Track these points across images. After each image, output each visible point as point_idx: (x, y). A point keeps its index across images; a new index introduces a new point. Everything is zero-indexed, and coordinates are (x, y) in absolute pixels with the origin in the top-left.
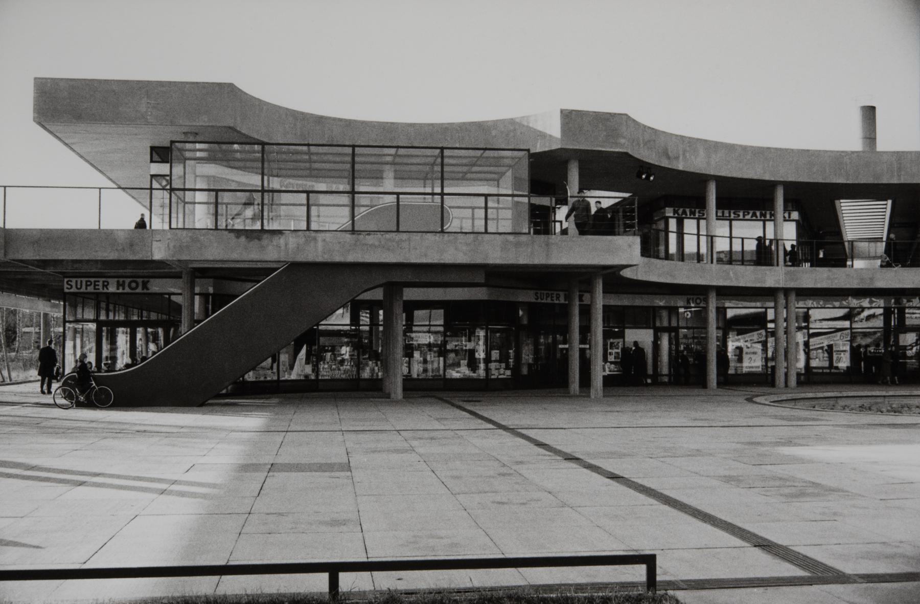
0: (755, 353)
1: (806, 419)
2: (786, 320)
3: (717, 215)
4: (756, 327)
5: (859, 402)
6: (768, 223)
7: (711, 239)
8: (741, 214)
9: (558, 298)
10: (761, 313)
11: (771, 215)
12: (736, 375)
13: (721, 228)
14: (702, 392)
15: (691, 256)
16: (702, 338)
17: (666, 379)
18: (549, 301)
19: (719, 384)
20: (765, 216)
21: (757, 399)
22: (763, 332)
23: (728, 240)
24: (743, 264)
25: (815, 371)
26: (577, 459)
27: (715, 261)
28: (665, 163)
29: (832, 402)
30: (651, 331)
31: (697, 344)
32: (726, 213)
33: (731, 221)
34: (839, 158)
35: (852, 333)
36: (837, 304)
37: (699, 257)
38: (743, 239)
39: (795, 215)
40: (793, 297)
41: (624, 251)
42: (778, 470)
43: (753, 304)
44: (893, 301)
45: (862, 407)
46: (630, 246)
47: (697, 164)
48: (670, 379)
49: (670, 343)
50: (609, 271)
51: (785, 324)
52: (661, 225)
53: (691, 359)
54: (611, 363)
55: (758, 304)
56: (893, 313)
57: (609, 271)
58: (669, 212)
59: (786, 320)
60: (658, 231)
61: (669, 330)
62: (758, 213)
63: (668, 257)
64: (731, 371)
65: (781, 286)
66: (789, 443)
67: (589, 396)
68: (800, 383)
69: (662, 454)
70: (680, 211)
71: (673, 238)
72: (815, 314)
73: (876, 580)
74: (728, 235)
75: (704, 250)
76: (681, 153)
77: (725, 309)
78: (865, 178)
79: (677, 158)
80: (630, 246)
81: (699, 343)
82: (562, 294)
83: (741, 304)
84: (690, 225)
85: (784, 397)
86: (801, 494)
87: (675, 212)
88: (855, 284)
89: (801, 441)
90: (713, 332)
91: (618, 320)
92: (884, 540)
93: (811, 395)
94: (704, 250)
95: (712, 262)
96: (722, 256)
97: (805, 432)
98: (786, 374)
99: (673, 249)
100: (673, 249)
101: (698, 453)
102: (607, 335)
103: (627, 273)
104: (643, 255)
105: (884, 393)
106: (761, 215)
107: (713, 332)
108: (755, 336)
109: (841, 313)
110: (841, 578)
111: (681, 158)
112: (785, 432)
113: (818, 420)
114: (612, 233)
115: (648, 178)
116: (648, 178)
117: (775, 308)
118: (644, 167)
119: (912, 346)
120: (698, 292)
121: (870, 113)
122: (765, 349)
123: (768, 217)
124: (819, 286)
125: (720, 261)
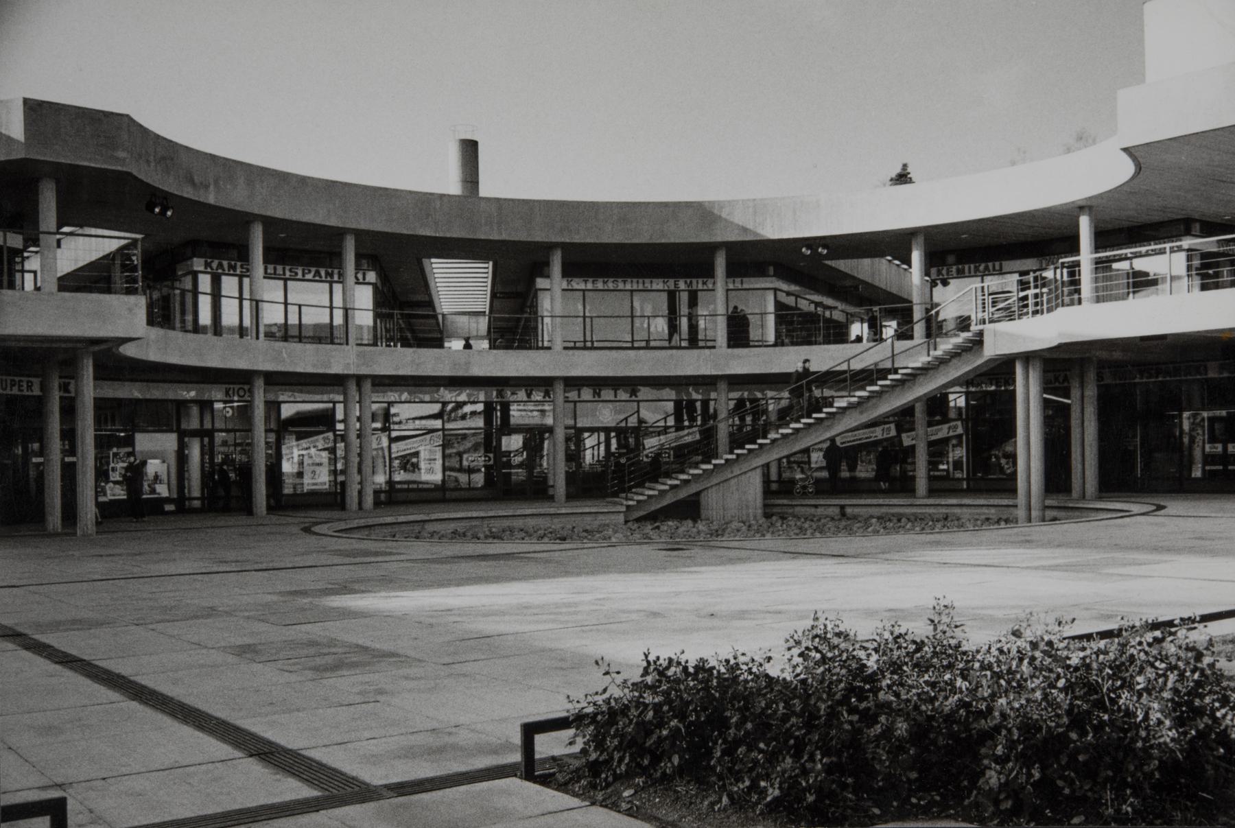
0: (320, 464)
1: (376, 554)
2: (359, 419)
3: (266, 272)
4: (321, 428)
5: (452, 526)
6: (335, 285)
7: (257, 304)
8: (300, 273)
9: (30, 387)
10: (327, 410)
11: (340, 275)
12: (295, 495)
13: (271, 291)
14: (243, 520)
15: (231, 330)
16: (248, 444)
17: (197, 504)
18: (15, 391)
19: (271, 509)
20: (332, 275)
21: (316, 529)
22: (330, 435)
23: (282, 307)
24: (300, 341)
25: (399, 486)
26: (20, 635)
27: (262, 335)
28: (188, 193)
29: (417, 528)
30: (173, 437)
31: (241, 453)
32: (280, 269)
33: (286, 280)
34: (425, 201)
35: (444, 435)
36: (427, 398)
37: (242, 331)
38: (300, 306)
39: (372, 276)
40: (367, 386)
41: (124, 317)
42: (316, 631)
43: (318, 397)
44: (495, 393)
45: (455, 532)
46: (130, 310)
47: (237, 198)
48: (203, 504)
49: (202, 454)
50: (103, 347)
51: (358, 425)
52: (187, 283)
53: (232, 475)
54: (116, 483)
55: (325, 398)
56: (495, 409)
57: (103, 347)
58: (198, 264)
59: (359, 419)
60: (183, 292)
61: (200, 433)
62: (323, 273)
63: (197, 329)
64: (288, 490)
65: (351, 372)
66: (345, 589)
67: (75, 534)
68: (377, 503)
69: (159, 617)
70: (215, 265)
71: (205, 303)
72: (403, 411)
73: (417, 788)
74: (282, 300)
75: (247, 322)
76: (211, 181)
77: (279, 404)
78: (457, 232)
79: (207, 187)
80: (130, 310)
81: (243, 452)
82: (36, 382)
83: (299, 397)
84: (229, 285)
85: (355, 524)
86: (336, 667)
87: (207, 265)
88: (445, 371)
89: (356, 587)
90: (260, 436)
91: (121, 421)
92: (435, 725)
93: (389, 520)
94: (247, 322)
95: (257, 338)
96: (274, 329)
97: (370, 572)
98: (360, 492)
99: (205, 317)
100: (205, 317)
101: (211, 612)
102: (103, 444)
103: (129, 350)
104: (151, 322)
105: (482, 514)
106: (327, 274)
107: (260, 436)
108: (320, 441)
109: (436, 408)
110: (362, 793)
111: (212, 188)
112: (342, 573)
113: (391, 554)
114: (109, 291)
115: (163, 212)
116: (163, 212)
117: (345, 402)
118: (156, 198)
119: (518, 452)
120: (239, 379)
121: (470, 149)
122: (333, 461)
123: (336, 278)
124: (401, 372)
125: (270, 335)
